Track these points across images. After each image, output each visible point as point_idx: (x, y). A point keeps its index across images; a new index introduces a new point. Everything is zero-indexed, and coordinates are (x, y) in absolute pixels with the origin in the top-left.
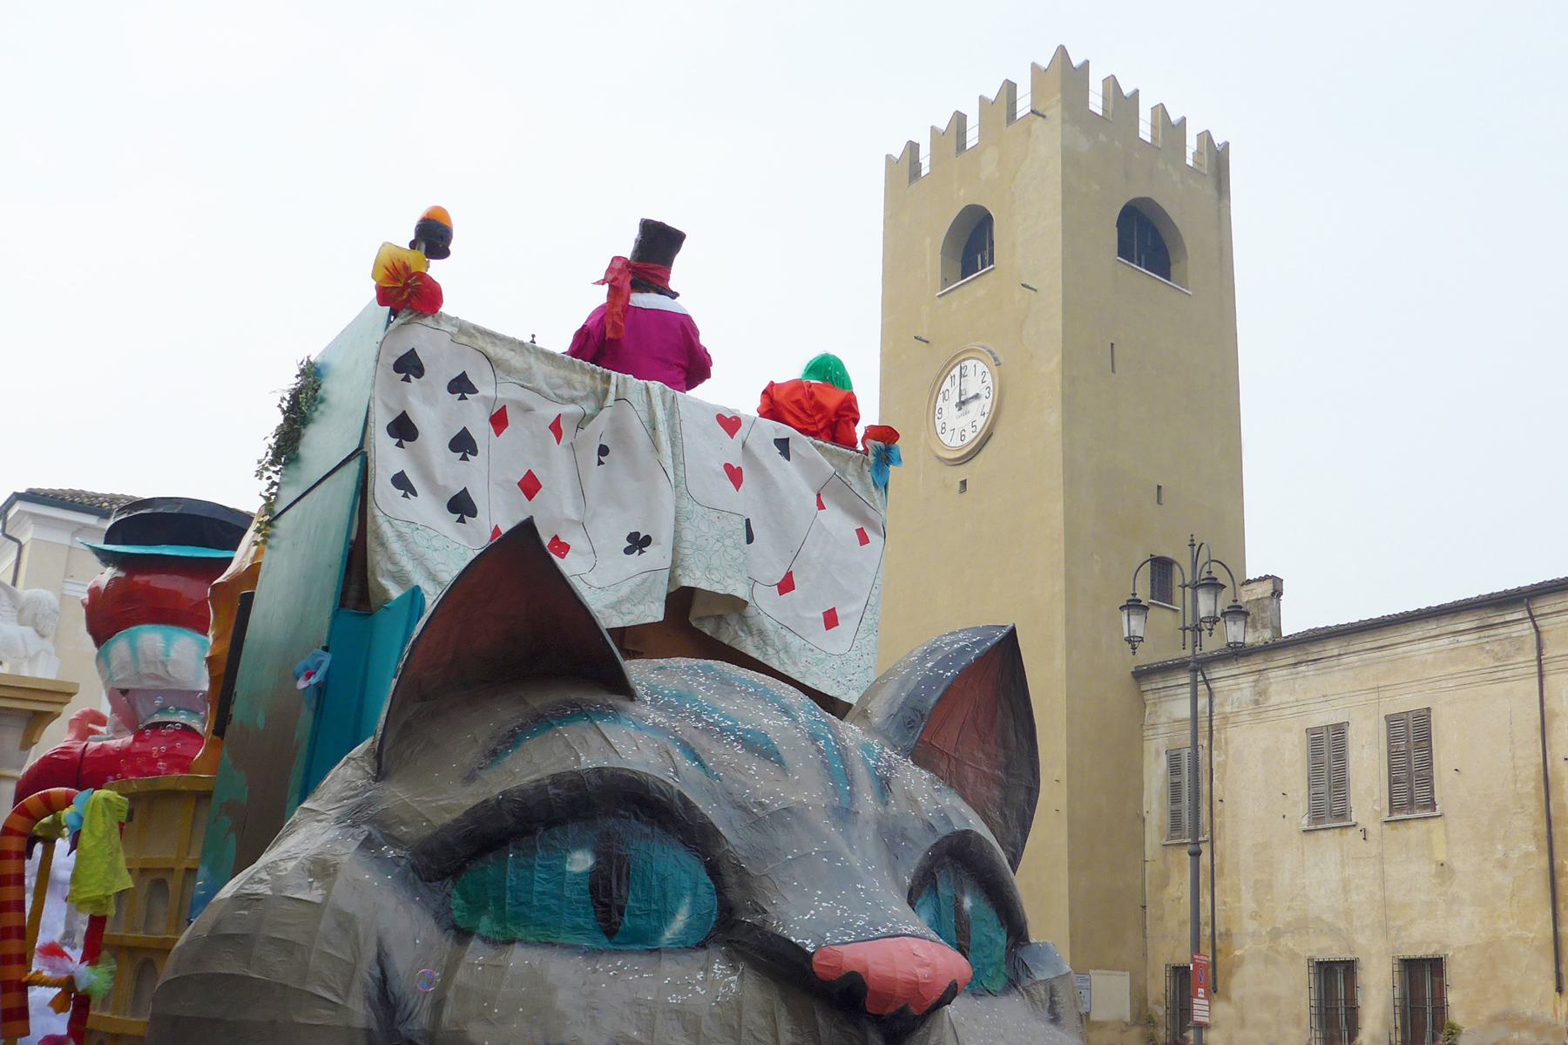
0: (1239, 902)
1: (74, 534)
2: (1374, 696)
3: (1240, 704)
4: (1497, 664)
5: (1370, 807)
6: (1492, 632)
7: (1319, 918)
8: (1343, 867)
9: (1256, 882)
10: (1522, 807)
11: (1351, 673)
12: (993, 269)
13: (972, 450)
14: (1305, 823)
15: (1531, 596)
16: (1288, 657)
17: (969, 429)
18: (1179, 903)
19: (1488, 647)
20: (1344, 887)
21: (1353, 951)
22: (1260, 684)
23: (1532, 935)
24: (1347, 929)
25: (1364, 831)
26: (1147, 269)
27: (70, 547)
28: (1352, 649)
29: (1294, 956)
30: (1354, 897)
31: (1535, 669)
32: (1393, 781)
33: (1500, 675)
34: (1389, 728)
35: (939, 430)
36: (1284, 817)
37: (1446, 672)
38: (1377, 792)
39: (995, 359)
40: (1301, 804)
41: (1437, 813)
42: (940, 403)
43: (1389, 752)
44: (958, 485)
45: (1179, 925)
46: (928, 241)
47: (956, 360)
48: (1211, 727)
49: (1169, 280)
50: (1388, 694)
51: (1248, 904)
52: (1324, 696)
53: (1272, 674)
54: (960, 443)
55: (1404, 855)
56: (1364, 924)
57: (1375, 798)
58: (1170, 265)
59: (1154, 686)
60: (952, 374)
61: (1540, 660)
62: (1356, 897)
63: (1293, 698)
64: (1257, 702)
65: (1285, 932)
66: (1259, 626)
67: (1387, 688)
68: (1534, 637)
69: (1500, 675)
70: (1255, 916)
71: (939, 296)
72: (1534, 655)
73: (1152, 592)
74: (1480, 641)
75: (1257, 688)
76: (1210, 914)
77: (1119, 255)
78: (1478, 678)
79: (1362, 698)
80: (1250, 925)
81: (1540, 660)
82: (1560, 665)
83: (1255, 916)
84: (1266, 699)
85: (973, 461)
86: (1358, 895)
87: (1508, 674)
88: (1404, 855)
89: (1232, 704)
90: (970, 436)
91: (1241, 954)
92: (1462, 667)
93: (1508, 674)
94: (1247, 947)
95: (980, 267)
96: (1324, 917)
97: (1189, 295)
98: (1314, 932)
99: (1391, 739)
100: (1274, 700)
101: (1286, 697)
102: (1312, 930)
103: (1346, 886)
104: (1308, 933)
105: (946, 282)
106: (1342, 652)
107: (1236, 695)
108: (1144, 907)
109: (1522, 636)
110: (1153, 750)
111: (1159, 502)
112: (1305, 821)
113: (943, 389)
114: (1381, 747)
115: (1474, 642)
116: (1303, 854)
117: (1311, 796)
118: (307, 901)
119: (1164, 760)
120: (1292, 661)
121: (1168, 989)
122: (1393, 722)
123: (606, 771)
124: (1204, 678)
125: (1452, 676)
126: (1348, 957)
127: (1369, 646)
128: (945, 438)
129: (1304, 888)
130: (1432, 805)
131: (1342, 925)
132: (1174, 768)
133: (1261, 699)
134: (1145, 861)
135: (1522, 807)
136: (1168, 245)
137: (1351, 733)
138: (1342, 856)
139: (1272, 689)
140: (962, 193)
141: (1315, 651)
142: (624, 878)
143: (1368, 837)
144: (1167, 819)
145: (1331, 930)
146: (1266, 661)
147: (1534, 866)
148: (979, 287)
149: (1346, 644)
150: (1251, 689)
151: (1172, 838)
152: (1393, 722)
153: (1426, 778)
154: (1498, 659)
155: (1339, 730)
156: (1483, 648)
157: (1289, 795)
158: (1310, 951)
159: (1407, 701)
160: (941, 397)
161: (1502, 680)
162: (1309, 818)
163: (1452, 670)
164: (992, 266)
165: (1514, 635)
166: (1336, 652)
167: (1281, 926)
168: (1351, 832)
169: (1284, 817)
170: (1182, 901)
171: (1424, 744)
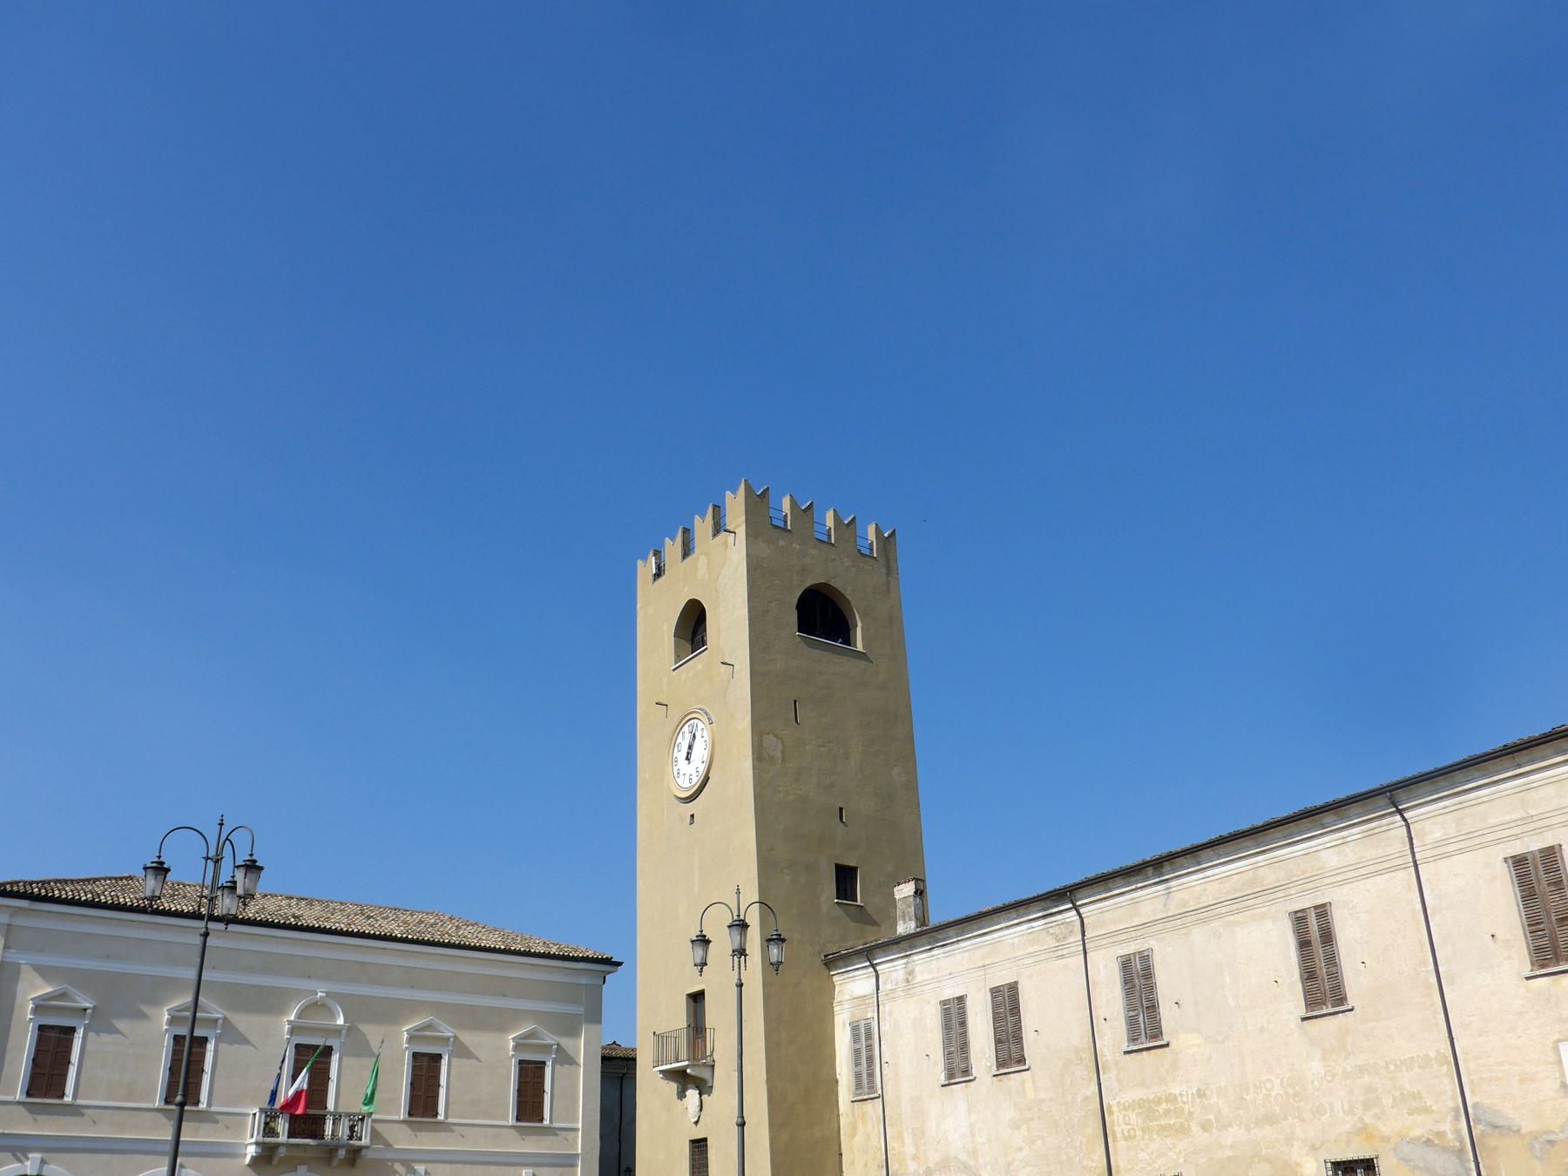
0: (904, 1146)
1: (11, 916)
2: (982, 973)
3: (897, 983)
4: (1058, 944)
6: (1053, 919)
7: (956, 1157)
9: (913, 1129)
10: (1081, 1059)
11: (967, 955)
12: (706, 649)
13: (695, 792)
14: (942, 1079)
15: (1073, 890)
17: (695, 774)
19: (1051, 931)
20: (971, 1131)
22: (909, 965)
23: (1094, 1165)
27: (8, 925)
30: (979, 1139)
31: (1081, 948)
32: (998, 1041)
33: (1060, 953)
34: (993, 998)
35: (676, 775)
37: (1027, 951)
38: (987, 1050)
39: (709, 719)
41: (1026, 1067)
42: (676, 754)
43: (994, 1019)
44: (689, 818)
46: (665, 627)
47: (686, 718)
48: (878, 1002)
49: (850, 646)
50: (991, 971)
51: (910, 1149)
52: (951, 974)
53: (915, 958)
54: (689, 785)
55: (1008, 1103)
58: (849, 630)
60: (683, 730)
61: (1083, 940)
63: (930, 977)
64: (907, 981)
65: (935, 1171)
66: (907, 919)
68: (1079, 922)
69: (1060, 953)
70: (915, 1158)
71: (674, 670)
72: (1080, 937)
73: (838, 893)
74: (1047, 926)
78: (1047, 956)
79: (974, 975)
81: (1083, 940)
82: (1097, 943)
83: (915, 1158)
84: (913, 978)
85: (698, 799)
87: (1065, 952)
88: (1008, 1103)
89: (892, 982)
90: (695, 780)
92: (1036, 948)
93: (1065, 952)
95: (701, 645)
96: (960, 1156)
99: (995, 1006)
100: (919, 978)
101: (926, 976)
105: (678, 657)
107: (894, 975)
109: (1072, 921)
112: (943, 1077)
113: (677, 742)
115: (1042, 927)
116: (943, 1105)
119: (848, 1029)
122: (995, 992)
123: (893, 910)
125: (1030, 955)
128: (680, 781)
130: (1022, 1060)
131: (972, 1163)
133: (910, 978)
135: (1081, 1059)
136: (847, 616)
137: (969, 1002)
138: (968, 1105)
139: (918, 969)
140: (686, 589)
142: (1111, 940)
144: (853, 1081)
145: (965, 1167)
147: (1091, 1107)
148: (699, 663)
150: (903, 970)
152: (995, 992)
153: (1018, 1038)
154: (1058, 941)
155: (1013, 988)
156: (1048, 932)
157: (931, 1056)
159: (1002, 978)
160: (676, 748)
161: (1062, 957)
163: (1030, 950)
164: (705, 647)
165: (1067, 920)
171: (1015, 1011)
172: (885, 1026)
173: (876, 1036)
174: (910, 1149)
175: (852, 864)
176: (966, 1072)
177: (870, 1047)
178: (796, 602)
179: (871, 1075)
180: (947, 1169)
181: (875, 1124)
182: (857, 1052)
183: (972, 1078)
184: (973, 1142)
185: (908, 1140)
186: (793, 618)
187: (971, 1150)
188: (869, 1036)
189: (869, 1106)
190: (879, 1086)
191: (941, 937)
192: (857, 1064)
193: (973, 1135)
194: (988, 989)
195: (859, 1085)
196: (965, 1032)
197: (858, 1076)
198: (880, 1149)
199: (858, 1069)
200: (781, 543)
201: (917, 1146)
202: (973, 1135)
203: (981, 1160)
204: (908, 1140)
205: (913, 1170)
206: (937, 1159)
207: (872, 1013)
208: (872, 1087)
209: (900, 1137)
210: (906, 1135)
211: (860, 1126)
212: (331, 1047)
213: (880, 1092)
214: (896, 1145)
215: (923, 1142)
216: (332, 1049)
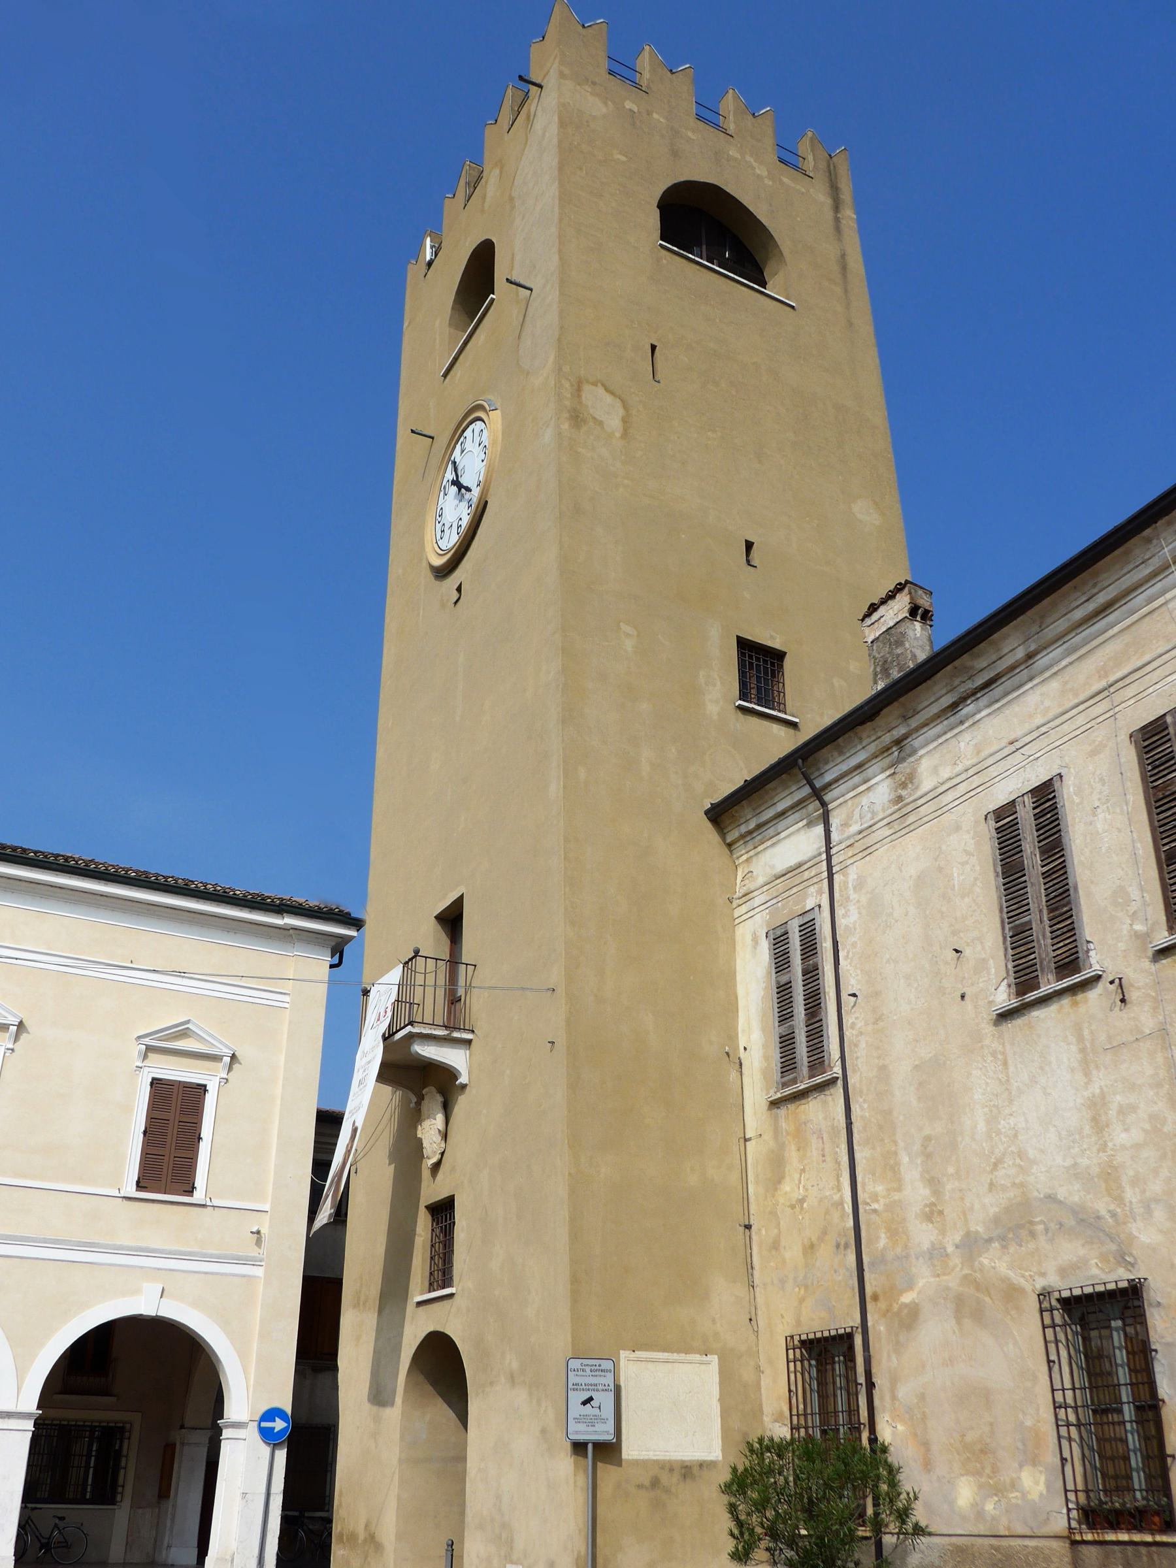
0: (899, 1189)
5: (1126, 927)
7: (1051, 1198)
8: (1087, 1074)
14: (1003, 998)
16: (937, 695)
18: (802, 1208)
20: (1095, 1119)
21: (1133, 1265)
24: (1113, 1215)
25: (1120, 983)
26: (720, 267)
28: (1051, 631)
29: (1011, 1293)
30: (1120, 1137)
36: (963, 997)
38: (1135, 893)
40: (991, 961)
45: (805, 1253)
51: (916, 1193)
56: (1148, 1194)
57: (1134, 907)
59: (743, 829)
62: (1123, 1135)
65: (990, 1240)
67: (1127, 681)
70: (932, 1213)
75: (897, 777)
76: (851, 1223)
77: (662, 239)
79: (1080, 720)
80: (923, 1235)
83: (932, 1213)
86: (1127, 1130)
89: (861, 818)
91: (913, 1302)
94: (921, 1283)
96: (1061, 1194)
97: (793, 307)
98: (1047, 1230)
102: (1040, 1227)
103: (1096, 1110)
104: (1033, 1234)
106: (1033, 647)
108: (748, 1227)
110: (749, 938)
111: (445, 375)
114: (1130, 798)
116: (1005, 1064)
117: (1005, 910)
118: (1098, 636)
120: (947, 701)
121: (793, 1388)
124: (812, 786)
126: (1116, 1277)
127: (1078, 614)
129: (1016, 1136)
131: (1102, 1206)
132: (781, 961)
134: (746, 1140)
138: (1083, 1050)
141: (983, 663)
143: (1133, 995)
146: (905, 718)
149: (1035, 628)
150: (889, 780)
151: (784, 1085)
157: (967, 952)
158: (1043, 1275)
162: (1009, 986)
166: (1020, 653)
167: (980, 1229)
168: (1093, 995)
169: (963, 997)
170: (805, 1205)
172: (845, 916)
173: (827, 945)
174: (916, 1193)
175: (776, 644)
176: (1069, 964)
177: (812, 973)
178: (682, 180)
179: (816, 1034)
180: (1024, 1233)
181: (828, 1147)
182: (784, 991)
183: (1085, 974)
184: (1103, 1148)
185: (911, 1173)
186: (653, 220)
187: (1095, 1170)
188: (810, 947)
189: (812, 1108)
190: (835, 1053)
191: (982, 663)
192: (785, 1014)
193: (1099, 1125)
194: (1124, 737)
195: (788, 1065)
196: (1063, 866)
197: (787, 1042)
198: (841, 1203)
199: (784, 979)
200: (629, 105)
201: (934, 1183)
202: (1099, 1125)
203: (1130, 1194)
204: (911, 1173)
205: (926, 1246)
206: (993, 1210)
207: (815, 897)
208: (818, 1061)
209: (891, 1169)
210: (905, 1159)
211: (792, 1154)
212: (205, 1086)
213: (837, 1069)
214: (880, 1188)
215: (951, 1170)
216: (205, 1091)
